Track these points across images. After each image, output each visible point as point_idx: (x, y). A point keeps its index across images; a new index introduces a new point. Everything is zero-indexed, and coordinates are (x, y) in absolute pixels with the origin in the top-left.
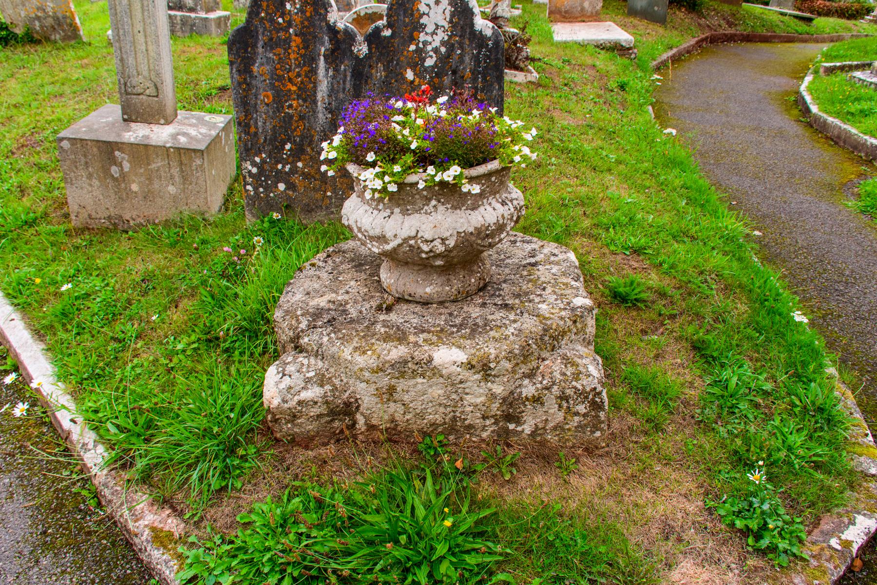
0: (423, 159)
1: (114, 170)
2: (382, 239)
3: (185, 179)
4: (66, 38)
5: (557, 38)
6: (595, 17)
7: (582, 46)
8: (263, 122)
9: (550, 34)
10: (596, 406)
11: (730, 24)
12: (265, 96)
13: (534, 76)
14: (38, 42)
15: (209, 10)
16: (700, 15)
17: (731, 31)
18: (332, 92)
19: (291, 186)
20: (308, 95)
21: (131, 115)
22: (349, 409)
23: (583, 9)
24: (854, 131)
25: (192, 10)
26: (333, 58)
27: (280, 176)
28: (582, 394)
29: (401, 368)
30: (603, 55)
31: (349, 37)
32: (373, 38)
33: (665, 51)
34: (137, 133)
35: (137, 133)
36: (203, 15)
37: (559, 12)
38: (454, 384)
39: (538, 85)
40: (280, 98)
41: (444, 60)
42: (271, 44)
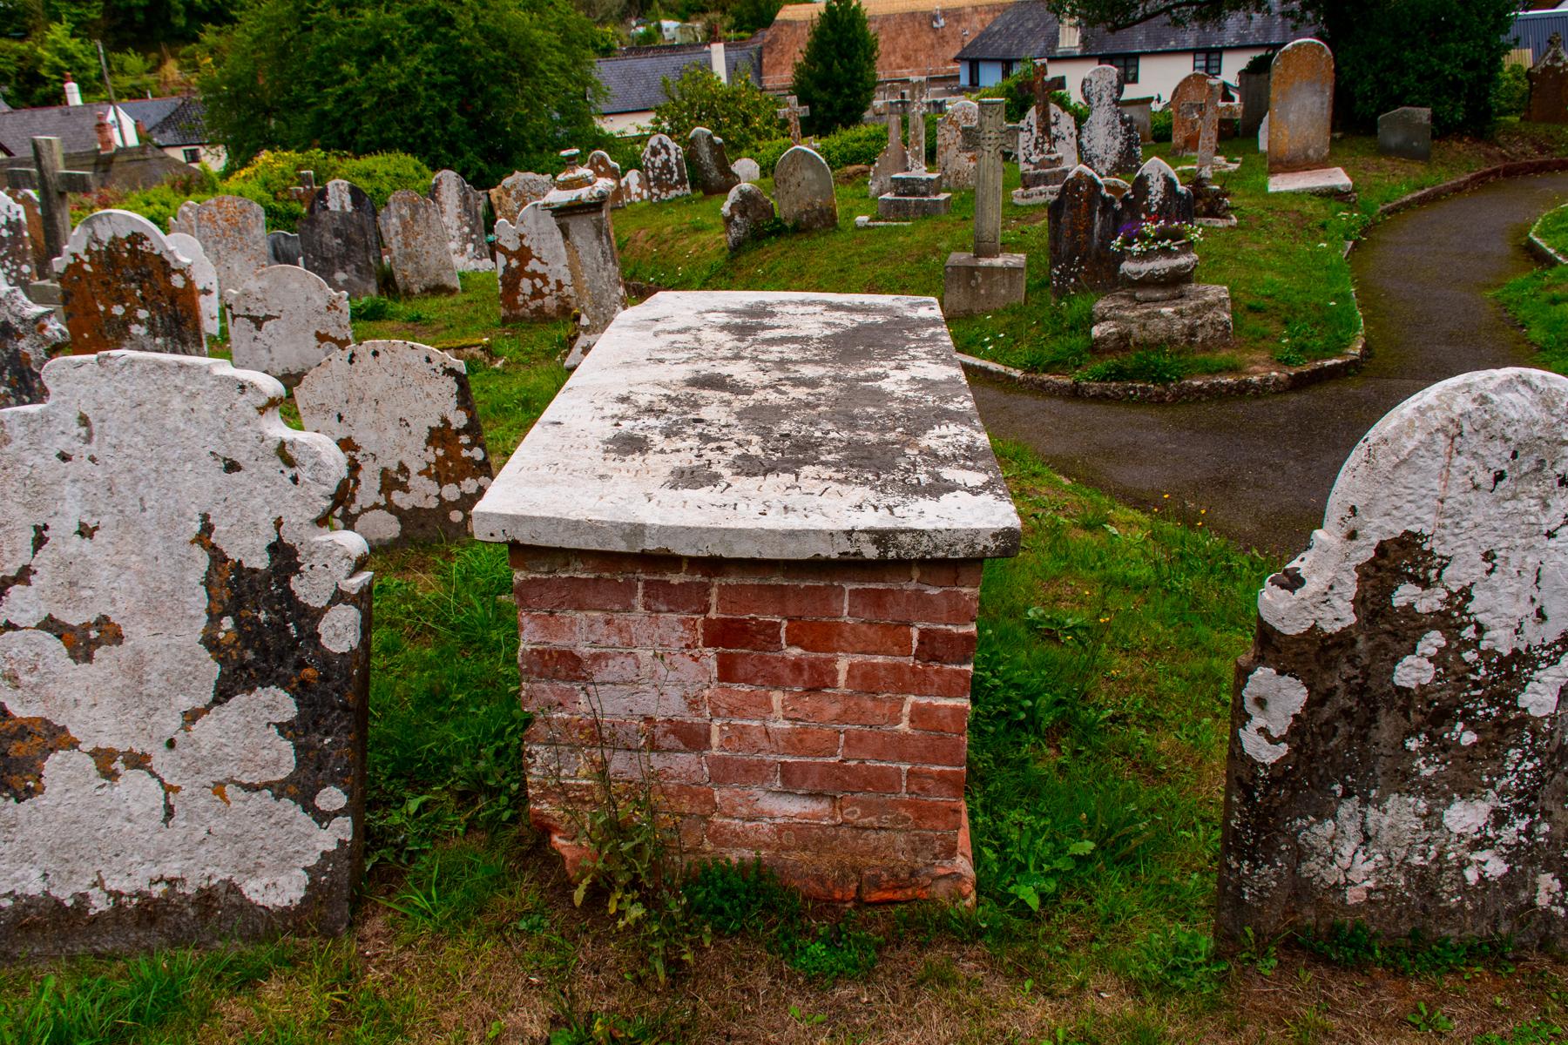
0: (1155, 240)
1: (973, 283)
2: (1139, 273)
3: (1011, 284)
4: (826, 225)
5: (1272, 189)
6: (1322, 164)
7: (1295, 194)
8: (1064, 247)
9: (1264, 186)
10: (1227, 328)
11: (1541, 150)
12: (1067, 233)
13: (1235, 221)
14: (804, 231)
15: (937, 194)
16: (1492, 142)
17: (1545, 158)
18: (1102, 228)
19: (1077, 280)
20: (1089, 230)
21: (980, 253)
22: (1129, 335)
23: (1307, 157)
24: (1544, 245)
25: (924, 194)
26: (1102, 212)
27: (1073, 275)
28: (1221, 323)
29: (1148, 316)
30: (1317, 201)
31: (1112, 201)
32: (1125, 200)
33: (1411, 191)
34: (984, 262)
35: (984, 262)
36: (933, 198)
37: (1281, 162)
38: (1169, 320)
39: (1238, 227)
40: (1074, 233)
41: (1160, 207)
42: (1071, 207)
